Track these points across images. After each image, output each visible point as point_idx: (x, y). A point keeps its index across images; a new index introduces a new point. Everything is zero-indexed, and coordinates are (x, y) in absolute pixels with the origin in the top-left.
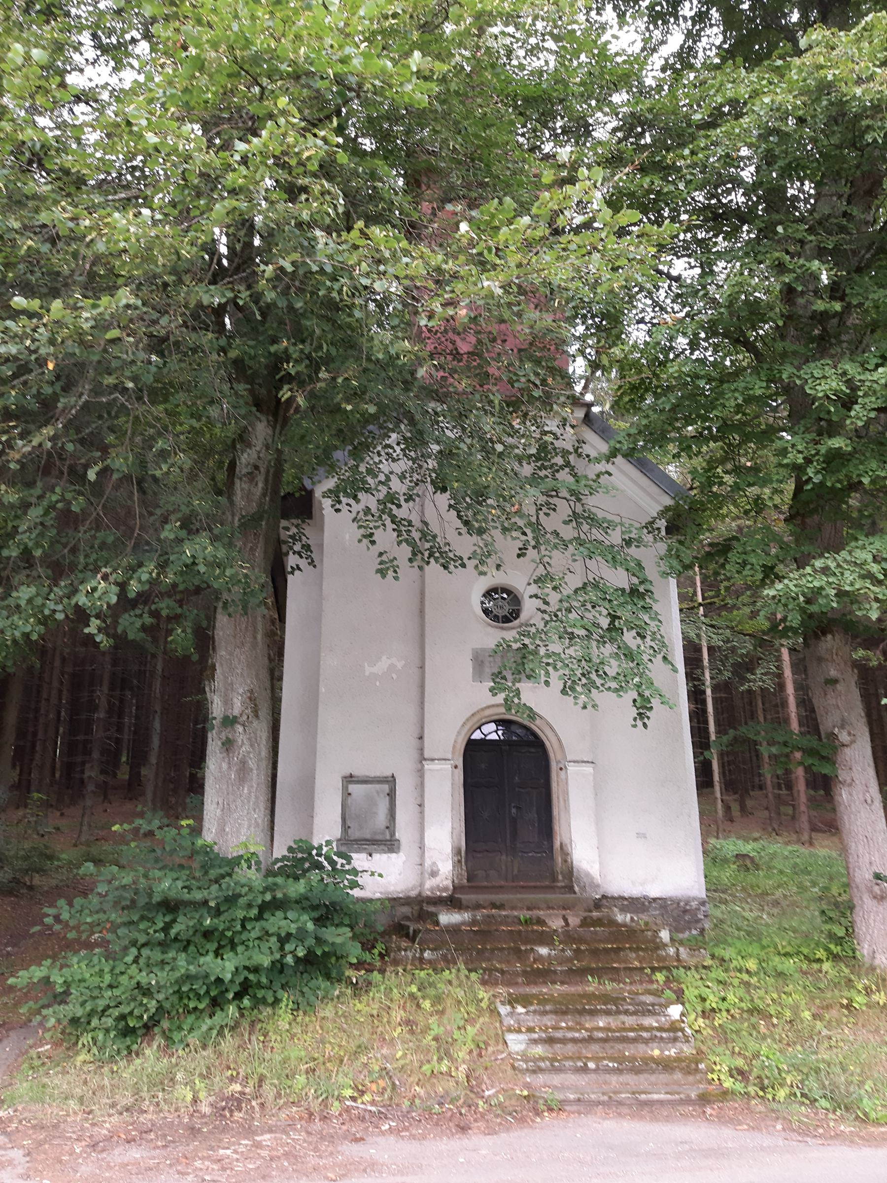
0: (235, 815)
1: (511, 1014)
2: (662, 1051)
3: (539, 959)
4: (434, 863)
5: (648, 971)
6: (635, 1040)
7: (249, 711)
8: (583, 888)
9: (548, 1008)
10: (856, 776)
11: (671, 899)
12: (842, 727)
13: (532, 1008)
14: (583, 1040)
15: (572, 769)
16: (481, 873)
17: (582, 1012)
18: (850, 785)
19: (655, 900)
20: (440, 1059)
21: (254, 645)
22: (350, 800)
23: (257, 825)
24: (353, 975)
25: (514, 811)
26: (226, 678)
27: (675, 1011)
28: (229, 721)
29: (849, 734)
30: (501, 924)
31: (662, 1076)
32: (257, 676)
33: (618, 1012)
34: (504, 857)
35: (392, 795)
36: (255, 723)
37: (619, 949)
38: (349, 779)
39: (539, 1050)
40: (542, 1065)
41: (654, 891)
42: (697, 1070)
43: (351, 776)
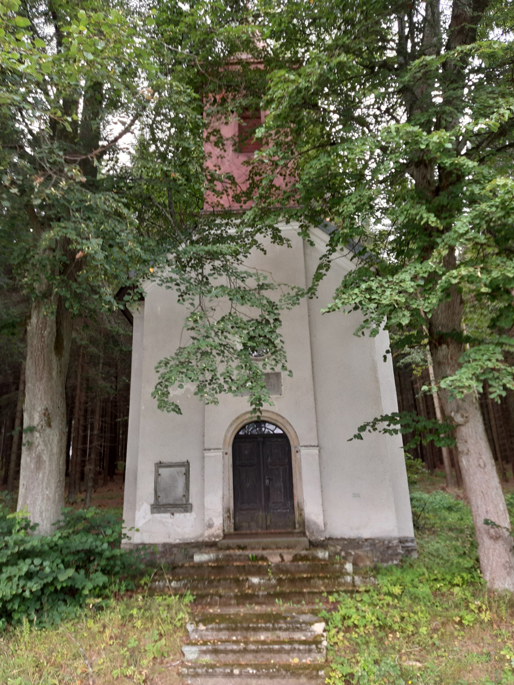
0: (33, 492)
1: (196, 630)
2: (300, 660)
3: (252, 586)
4: (211, 519)
5: (325, 594)
6: (279, 651)
7: (43, 423)
8: (312, 533)
9: (222, 626)
10: (472, 448)
11: (378, 539)
12: (457, 412)
13: (210, 626)
14: (239, 651)
15: (303, 451)
16: (245, 524)
17: (248, 629)
18: (467, 454)
19: (366, 540)
20: (129, 665)
21: (50, 378)
22: (159, 478)
23: (49, 498)
24: (92, 601)
25: (267, 481)
26: (31, 401)
27: (319, 628)
28: (32, 429)
29: (462, 416)
30: (236, 560)
31: (290, 680)
32: (51, 399)
33: (274, 629)
34: (260, 513)
35: (187, 474)
36: (48, 430)
37: (311, 578)
38: (160, 465)
39: (207, 659)
40: (199, 671)
41: (366, 534)
42: (318, 676)
43: (160, 463)
